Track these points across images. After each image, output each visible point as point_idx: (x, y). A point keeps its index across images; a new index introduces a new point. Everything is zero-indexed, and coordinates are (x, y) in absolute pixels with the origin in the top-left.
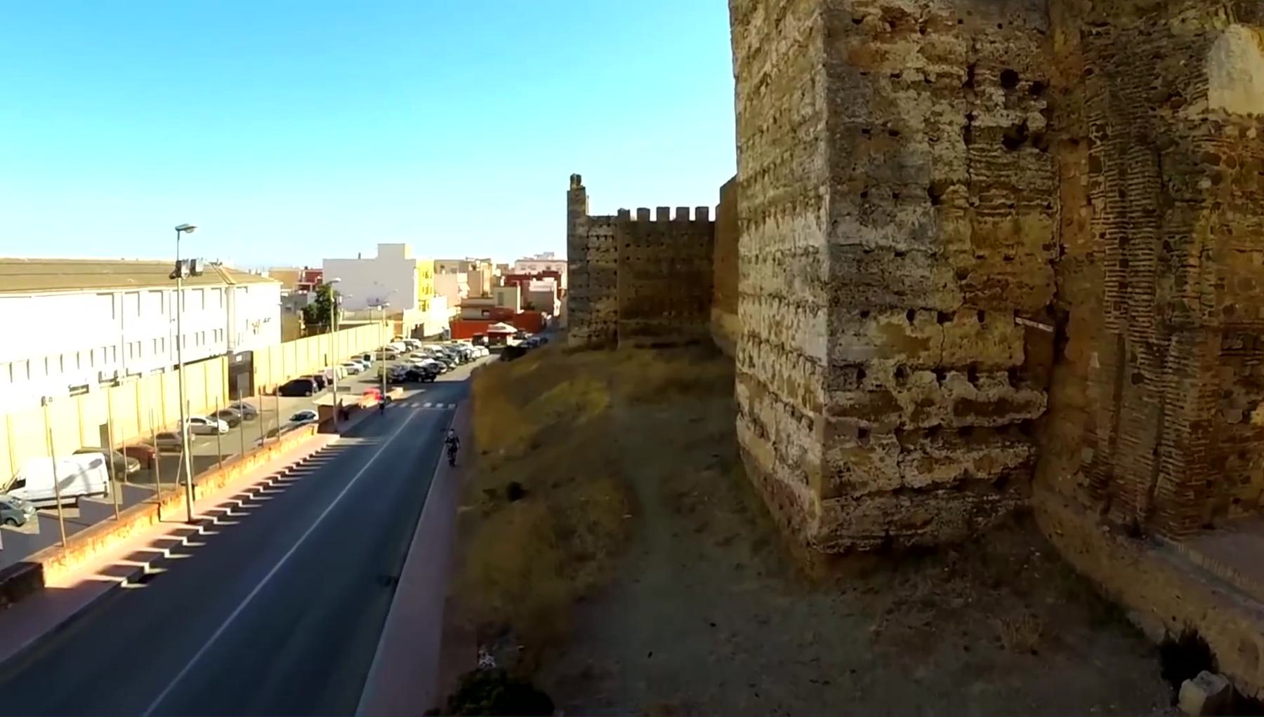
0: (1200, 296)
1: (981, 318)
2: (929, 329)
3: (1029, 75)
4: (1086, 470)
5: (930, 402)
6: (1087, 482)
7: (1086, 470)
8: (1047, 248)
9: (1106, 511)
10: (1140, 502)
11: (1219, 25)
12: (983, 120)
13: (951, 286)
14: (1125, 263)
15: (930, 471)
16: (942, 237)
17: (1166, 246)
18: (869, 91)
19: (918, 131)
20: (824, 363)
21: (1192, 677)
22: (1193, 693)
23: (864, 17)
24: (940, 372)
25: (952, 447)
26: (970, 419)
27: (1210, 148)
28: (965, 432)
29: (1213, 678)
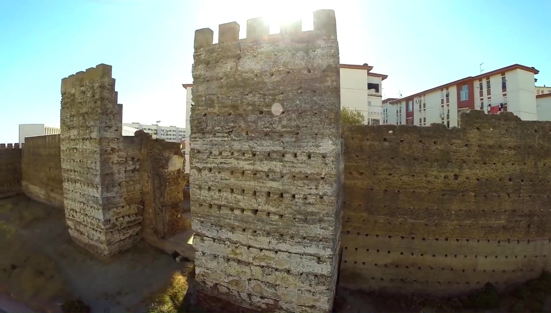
0: (167, 200)
1: (129, 206)
2: (120, 210)
3: (137, 158)
4: (152, 229)
5: (122, 223)
6: (153, 231)
7: (152, 229)
8: (140, 190)
11: (171, 155)
12: (128, 168)
13: (123, 201)
16: (121, 192)
19: (116, 173)
20: (103, 220)
21: (177, 257)
22: (178, 259)
24: (123, 217)
25: (127, 230)
27: (168, 177)
28: (129, 227)
29: (180, 256)
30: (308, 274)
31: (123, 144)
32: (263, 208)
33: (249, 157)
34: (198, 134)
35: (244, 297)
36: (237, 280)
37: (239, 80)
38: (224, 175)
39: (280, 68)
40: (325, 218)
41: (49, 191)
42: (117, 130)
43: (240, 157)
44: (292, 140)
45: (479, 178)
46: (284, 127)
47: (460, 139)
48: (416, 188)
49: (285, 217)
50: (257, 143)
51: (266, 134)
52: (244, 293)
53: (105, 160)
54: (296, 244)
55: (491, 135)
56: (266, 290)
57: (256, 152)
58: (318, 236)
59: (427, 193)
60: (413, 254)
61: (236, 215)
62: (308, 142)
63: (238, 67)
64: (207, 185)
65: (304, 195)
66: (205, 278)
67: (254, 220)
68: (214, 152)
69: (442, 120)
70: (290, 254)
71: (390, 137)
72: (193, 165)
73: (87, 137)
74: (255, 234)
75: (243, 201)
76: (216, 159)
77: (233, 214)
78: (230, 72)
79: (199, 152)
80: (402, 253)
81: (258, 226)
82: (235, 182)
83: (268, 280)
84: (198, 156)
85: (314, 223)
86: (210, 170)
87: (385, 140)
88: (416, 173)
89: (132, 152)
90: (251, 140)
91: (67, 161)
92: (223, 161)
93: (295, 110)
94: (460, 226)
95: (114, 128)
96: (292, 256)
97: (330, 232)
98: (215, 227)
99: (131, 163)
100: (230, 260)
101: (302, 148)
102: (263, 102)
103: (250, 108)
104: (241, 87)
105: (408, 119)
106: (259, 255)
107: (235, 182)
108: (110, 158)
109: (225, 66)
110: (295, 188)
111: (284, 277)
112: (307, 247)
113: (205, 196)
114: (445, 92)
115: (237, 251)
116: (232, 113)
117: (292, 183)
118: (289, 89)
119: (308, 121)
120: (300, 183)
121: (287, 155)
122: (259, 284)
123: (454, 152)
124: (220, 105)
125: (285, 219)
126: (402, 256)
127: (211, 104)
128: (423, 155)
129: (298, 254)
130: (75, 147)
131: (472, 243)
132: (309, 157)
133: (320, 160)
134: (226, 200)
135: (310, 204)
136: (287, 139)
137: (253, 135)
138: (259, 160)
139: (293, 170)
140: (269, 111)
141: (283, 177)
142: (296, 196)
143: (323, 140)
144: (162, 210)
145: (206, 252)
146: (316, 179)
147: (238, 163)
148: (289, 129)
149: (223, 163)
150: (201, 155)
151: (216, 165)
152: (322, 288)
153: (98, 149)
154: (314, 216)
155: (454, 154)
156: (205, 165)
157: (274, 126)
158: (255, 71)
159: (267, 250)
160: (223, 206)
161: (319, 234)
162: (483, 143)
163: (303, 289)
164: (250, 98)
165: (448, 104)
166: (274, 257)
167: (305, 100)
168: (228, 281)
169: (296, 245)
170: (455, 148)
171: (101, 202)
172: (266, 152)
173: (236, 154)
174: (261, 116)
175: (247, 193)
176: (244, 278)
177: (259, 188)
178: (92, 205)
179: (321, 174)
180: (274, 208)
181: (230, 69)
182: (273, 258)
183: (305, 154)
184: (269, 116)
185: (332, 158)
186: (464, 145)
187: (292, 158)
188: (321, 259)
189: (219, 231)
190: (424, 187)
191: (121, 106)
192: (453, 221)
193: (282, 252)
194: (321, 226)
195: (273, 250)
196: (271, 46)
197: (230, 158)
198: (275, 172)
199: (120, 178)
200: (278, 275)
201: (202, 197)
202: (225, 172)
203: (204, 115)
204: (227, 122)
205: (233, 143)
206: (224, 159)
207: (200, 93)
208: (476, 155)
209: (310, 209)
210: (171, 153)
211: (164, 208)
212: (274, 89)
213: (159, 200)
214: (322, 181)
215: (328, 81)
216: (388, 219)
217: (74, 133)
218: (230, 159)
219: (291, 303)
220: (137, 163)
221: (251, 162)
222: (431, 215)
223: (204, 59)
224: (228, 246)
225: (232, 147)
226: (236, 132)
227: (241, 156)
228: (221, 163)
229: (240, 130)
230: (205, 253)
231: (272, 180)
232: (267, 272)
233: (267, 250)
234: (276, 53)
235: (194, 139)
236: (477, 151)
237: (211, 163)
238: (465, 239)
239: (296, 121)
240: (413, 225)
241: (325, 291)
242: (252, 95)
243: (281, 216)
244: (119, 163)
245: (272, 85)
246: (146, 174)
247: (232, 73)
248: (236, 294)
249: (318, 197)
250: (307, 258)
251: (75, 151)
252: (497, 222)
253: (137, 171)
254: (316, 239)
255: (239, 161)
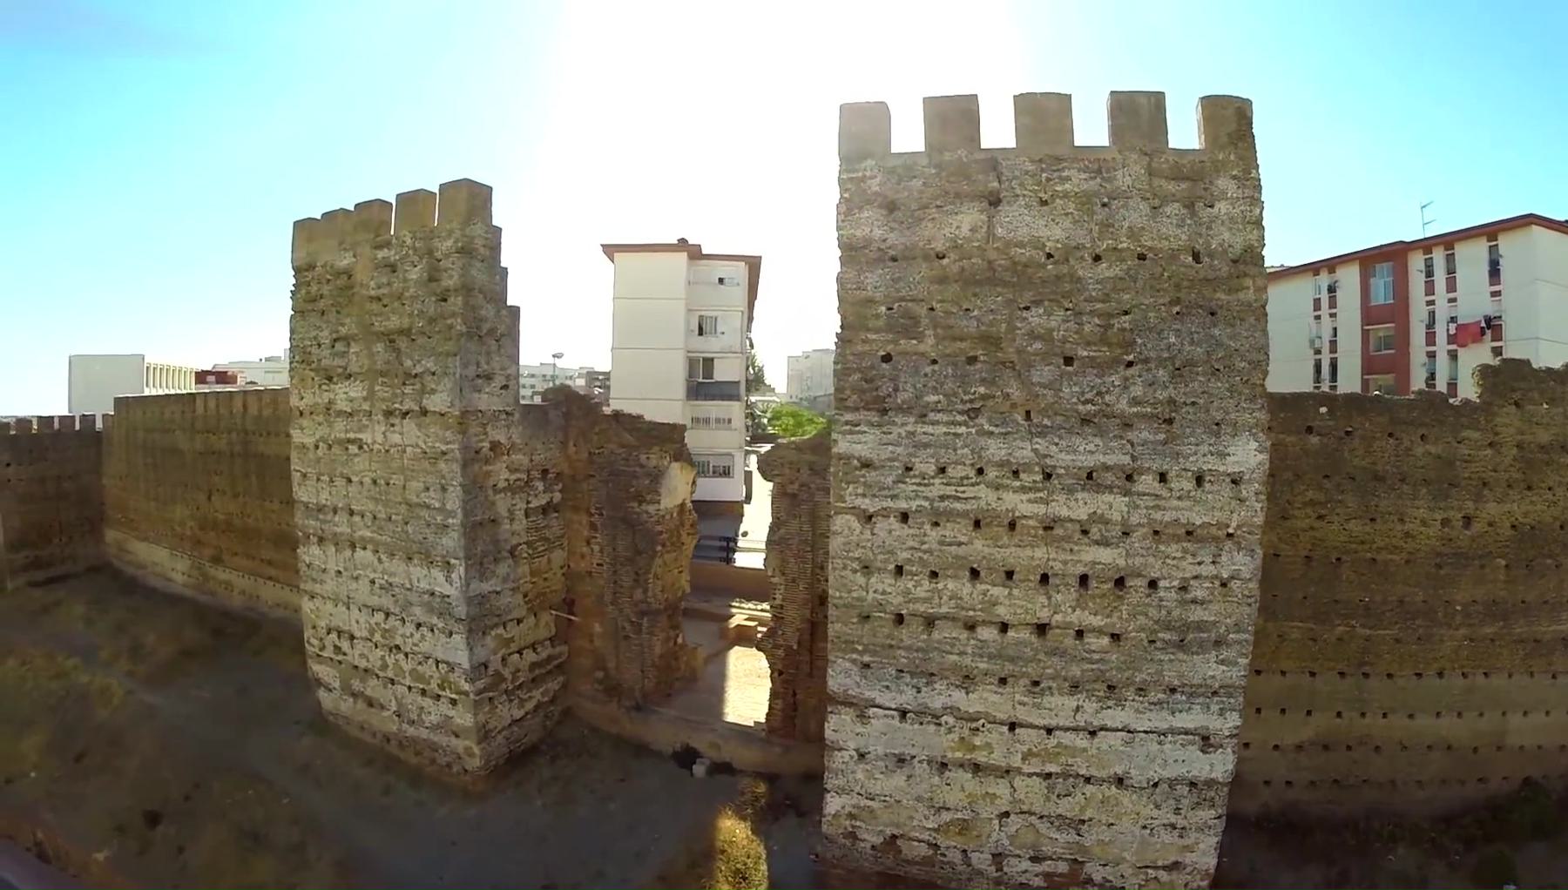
1: (535, 615)
4: (600, 682)
6: (601, 688)
8: (562, 568)
9: (619, 701)
10: (637, 694)
14: (615, 582)
15: (523, 707)
17: (637, 574)
18: (482, 499)
21: (695, 763)
22: (699, 769)
23: (481, 449)
24: (520, 652)
25: (530, 690)
26: (537, 672)
27: (659, 528)
28: (533, 680)
30: (1172, 783)
31: (521, 428)
32: (1068, 619)
33: (1034, 481)
34: (866, 413)
35: (981, 864)
36: (965, 820)
37: (1000, 265)
38: (949, 531)
39: (1121, 243)
40: (1231, 636)
41: (207, 564)
42: (505, 387)
43: (1005, 481)
44: (1157, 438)
45: (1516, 523)
46: (1135, 402)
47: (1479, 430)
48: (1379, 549)
49: (1127, 639)
50: (1057, 444)
51: (1086, 421)
52: (982, 853)
53: (474, 482)
54: (1152, 707)
55: (1544, 421)
56: (1051, 838)
57: (1054, 467)
58: (1209, 682)
59: (1403, 561)
60: (1363, 715)
61: (981, 641)
62: (1197, 445)
63: (994, 227)
64: (892, 559)
65: (1184, 579)
66: (858, 823)
67: (1036, 651)
68: (919, 467)
69: (1316, 354)
70: (1131, 735)
71: (1321, 423)
72: (845, 502)
73: (405, 408)
74: (1037, 689)
75: (1008, 603)
76: (925, 485)
77: (973, 638)
78: (968, 240)
79: (867, 465)
80: (1339, 715)
81: (1048, 668)
82: (987, 550)
83: (1059, 811)
84: (864, 476)
85: (1202, 648)
86: (904, 517)
87: (1310, 430)
88: (1382, 513)
89: (546, 453)
90: (1042, 435)
91: (318, 480)
92: (948, 493)
93: (1166, 359)
94: (1472, 640)
95: (499, 381)
96: (1137, 740)
97: (1239, 671)
98: (912, 678)
99: (540, 486)
100: (949, 767)
101: (1181, 460)
102: (1076, 333)
103: (1038, 345)
104: (1005, 284)
105: (1368, 380)
106: (1043, 747)
107: (987, 550)
108: (488, 474)
109: (954, 221)
110: (1160, 562)
111: (1109, 797)
112: (1181, 712)
113: (884, 593)
114: (1324, 279)
115: (977, 741)
116: (982, 358)
117: (1150, 551)
118: (1147, 302)
119: (1201, 390)
120: (1174, 549)
121: (1143, 477)
122: (1032, 824)
123: (1466, 462)
124: (939, 331)
125: (1126, 645)
126: (1338, 720)
127: (907, 326)
128: (1397, 467)
129: (1154, 732)
130: (352, 435)
131: (1498, 681)
132: (1199, 480)
133: (1227, 490)
134: (953, 601)
135: (1194, 601)
136: (1143, 434)
137: (1046, 422)
138: (1063, 489)
139: (1158, 516)
140: (1093, 357)
141: (1128, 534)
142: (1162, 584)
143: (1237, 438)
144: (641, 625)
145: (871, 748)
146: (1216, 539)
147: (999, 499)
148: (1149, 410)
149: (949, 497)
150: (873, 474)
151: (926, 504)
152: (1206, 814)
153: (456, 446)
154: (1203, 632)
155: (1465, 465)
156: (889, 503)
157: (1107, 398)
158: (1048, 244)
159: (1067, 729)
160: (938, 619)
161: (1213, 677)
162: (1528, 438)
163: (1156, 822)
164: (1036, 318)
165: (1334, 311)
166: (1084, 746)
167: (1192, 333)
168: (936, 826)
169: (1151, 710)
170: (1467, 452)
171: (461, 610)
172: (1084, 467)
173: (992, 474)
174: (1070, 369)
175: (1024, 581)
176: (987, 811)
177: (1058, 566)
178: (422, 619)
179: (1228, 526)
180: (1099, 617)
181: (970, 230)
182: (1085, 750)
183: (1190, 474)
184: (1095, 372)
185: (1256, 485)
186: (1486, 443)
187: (1156, 484)
188: (1212, 741)
189: (924, 689)
190: (1396, 548)
191: (515, 311)
192: (1457, 629)
193: (1109, 733)
194: (1221, 657)
195: (1084, 729)
196: (1091, 178)
197: (973, 485)
198: (1107, 522)
199: (513, 534)
200: (1092, 794)
201: (871, 595)
202: (954, 521)
203: (883, 357)
204: (964, 381)
205: (983, 441)
206: (954, 488)
207: (870, 293)
208: (1512, 469)
209: (1197, 614)
210: (664, 455)
211: (645, 619)
212: (1106, 299)
213: (631, 597)
214: (1229, 544)
215: (1248, 288)
216: (1312, 629)
217: (347, 394)
218: (971, 488)
219: (1118, 865)
220: (556, 487)
221: (1039, 495)
222: (1408, 616)
223: (876, 193)
224: (949, 729)
225: (979, 453)
226: (996, 412)
227: (1008, 478)
228: (942, 498)
229: (1006, 407)
230: (869, 753)
231: (1098, 544)
232: (1059, 789)
233: (1067, 729)
234: (1106, 200)
235: (848, 427)
236: (1515, 459)
237: (908, 498)
238: (1482, 671)
239: (1167, 387)
240: (1367, 643)
241: (1210, 823)
242: (1041, 311)
243: (1115, 637)
244: (511, 489)
245: (1100, 287)
246: (585, 519)
247: (976, 244)
248: (956, 857)
249: (1217, 583)
250: (1175, 742)
251: (353, 449)
252: (1551, 629)
253: (557, 512)
254: (1203, 690)
255: (1001, 492)
